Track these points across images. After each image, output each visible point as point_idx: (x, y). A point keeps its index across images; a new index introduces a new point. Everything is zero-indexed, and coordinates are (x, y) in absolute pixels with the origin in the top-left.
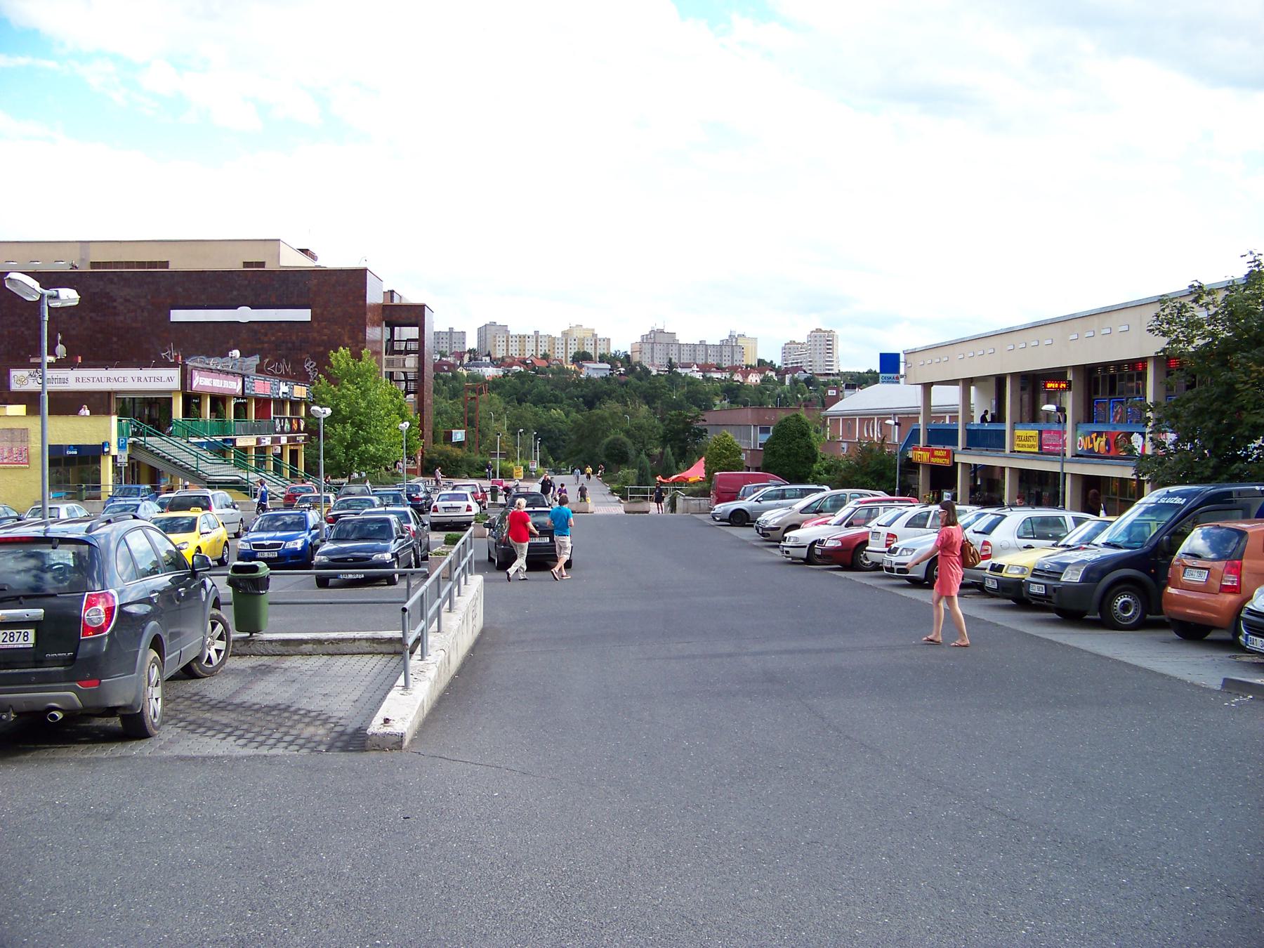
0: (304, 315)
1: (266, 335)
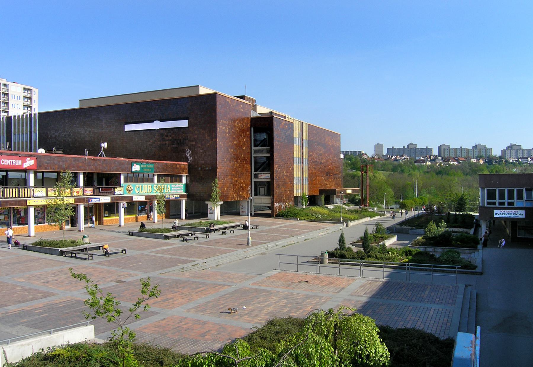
0: (185, 123)
1: (167, 136)
